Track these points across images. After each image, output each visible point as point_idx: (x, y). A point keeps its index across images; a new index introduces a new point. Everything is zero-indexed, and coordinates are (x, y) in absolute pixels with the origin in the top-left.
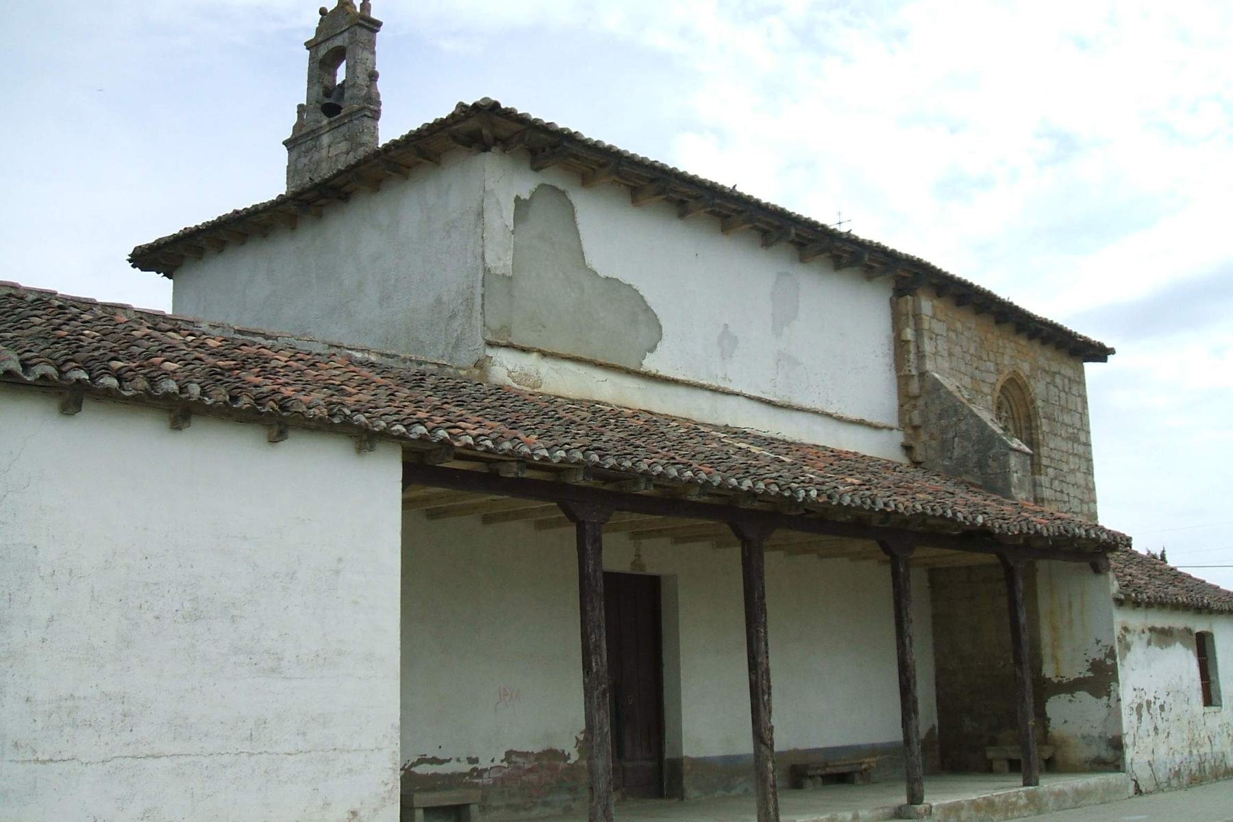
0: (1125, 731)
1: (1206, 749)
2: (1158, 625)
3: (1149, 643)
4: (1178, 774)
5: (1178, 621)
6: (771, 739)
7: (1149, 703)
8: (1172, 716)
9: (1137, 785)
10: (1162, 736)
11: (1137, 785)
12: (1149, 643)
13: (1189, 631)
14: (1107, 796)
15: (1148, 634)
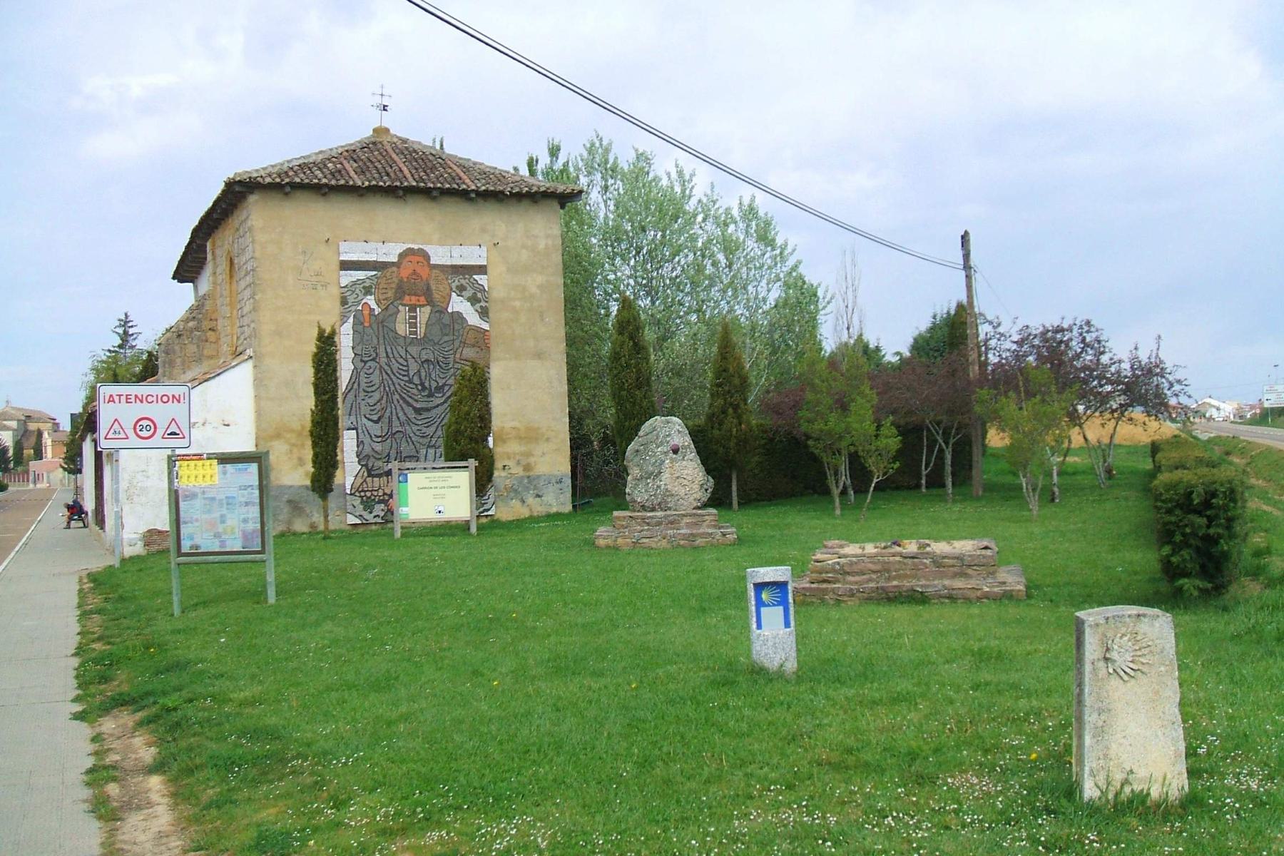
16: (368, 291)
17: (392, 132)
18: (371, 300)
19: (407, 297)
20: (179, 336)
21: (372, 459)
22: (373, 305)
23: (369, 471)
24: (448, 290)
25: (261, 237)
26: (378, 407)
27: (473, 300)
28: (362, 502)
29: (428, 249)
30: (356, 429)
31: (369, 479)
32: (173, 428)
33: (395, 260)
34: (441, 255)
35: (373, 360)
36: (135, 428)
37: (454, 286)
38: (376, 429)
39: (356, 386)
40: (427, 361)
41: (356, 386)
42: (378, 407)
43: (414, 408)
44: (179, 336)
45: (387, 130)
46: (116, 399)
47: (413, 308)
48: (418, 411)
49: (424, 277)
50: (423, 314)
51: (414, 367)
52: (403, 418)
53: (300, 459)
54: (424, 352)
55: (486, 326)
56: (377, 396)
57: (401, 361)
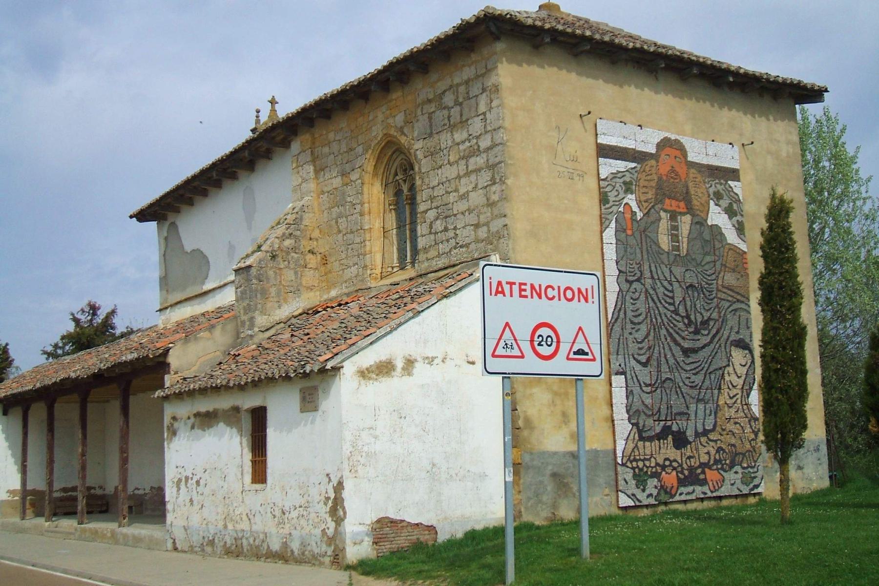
0: (167, 500)
1: (244, 525)
2: (203, 409)
3: (193, 427)
4: (212, 543)
5: (224, 403)
6: (574, 16)
7: (187, 478)
8: (207, 491)
9: (174, 543)
10: (196, 507)
11: (174, 543)
12: (193, 427)
13: (236, 409)
14: (152, 545)
15: (192, 420)
16: (628, 188)
17: (562, 9)
18: (631, 200)
19: (667, 201)
20: (274, 257)
21: (643, 417)
22: (635, 208)
23: (640, 432)
24: (705, 198)
25: (510, 100)
26: (645, 345)
27: (731, 212)
28: (635, 476)
29: (686, 141)
30: (623, 373)
31: (640, 444)
32: (580, 345)
33: (654, 151)
34: (700, 151)
35: (638, 280)
36: (532, 341)
37: (711, 190)
38: (645, 375)
39: (622, 315)
40: (691, 286)
41: (622, 315)
42: (645, 345)
43: (682, 348)
44: (274, 257)
45: (557, 7)
46: (507, 288)
47: (673, 217)
48: (686, 352)
49: (683, 176)
50: (685, 223)
51: (679, 294)
52: (672, 361)
53: (564, 414)
54: (688, 275)
55: (743, 247)
56: (644, 328)
57: (666, 283)
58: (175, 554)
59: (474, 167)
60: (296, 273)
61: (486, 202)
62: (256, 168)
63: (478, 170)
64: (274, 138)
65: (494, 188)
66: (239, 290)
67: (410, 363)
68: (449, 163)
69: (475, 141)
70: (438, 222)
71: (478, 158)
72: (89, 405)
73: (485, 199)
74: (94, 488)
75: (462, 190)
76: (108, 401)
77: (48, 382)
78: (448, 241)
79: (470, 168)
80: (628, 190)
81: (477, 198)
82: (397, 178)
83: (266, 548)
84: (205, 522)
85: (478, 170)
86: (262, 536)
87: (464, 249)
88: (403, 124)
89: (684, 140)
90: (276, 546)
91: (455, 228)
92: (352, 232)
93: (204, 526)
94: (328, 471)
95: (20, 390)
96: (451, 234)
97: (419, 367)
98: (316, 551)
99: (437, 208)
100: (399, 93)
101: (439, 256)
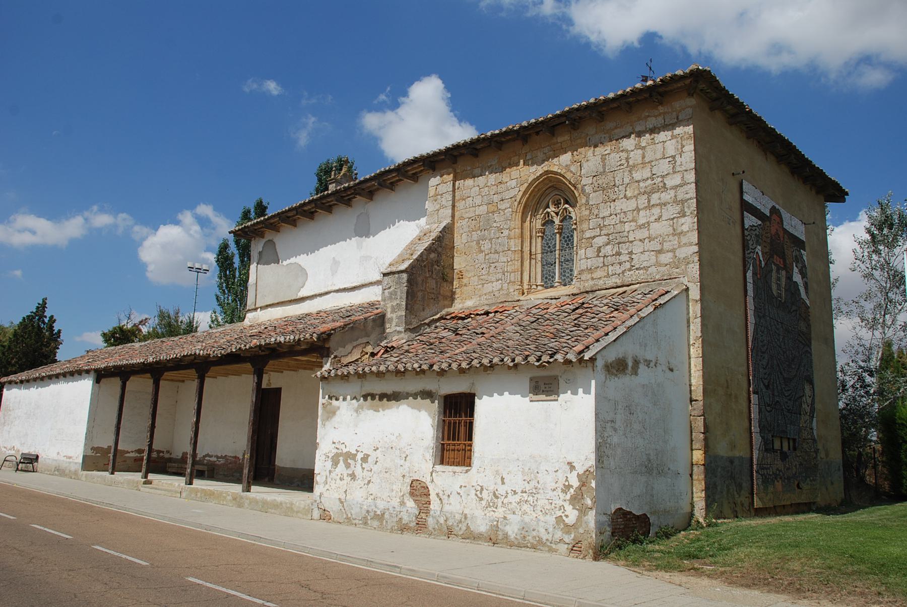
58: (323, 524)
59: (658, 201)
60: (437, 283)
61: (672, 231)
62: (375, 197)
63: (663, 205)
64: (407, 171)
65: (683, 220)
66: (386, 291)
67: (636, 363)
68: (625, 196)
69: (660, 179)
70: (609, 247)
71: (664, 194)
72: (162, 383)
73: (671, 228)
74: (163, 452)
75: (642, 221)
76: (183, 381)
77: (163, 357)
78: (620, 264)
79: (652, 203)
80: (758, 243)
81: (658, 228)
82: (548, 210)
83: (464, 528)
84: (372, 497)
85: (663, 205)
86: (458, 517)
87: (641, 272)
88: (569, 163)
89: (782, 210)
90: (481, 526)
91: (631, 253)
92: (496, 252)
93: (370, 500)
94: (570, 459)
95: (125, 362)
96: (624, 258)
97: (642, 368)
98: (545, 536)
99: (608, 235)
100: (567, 137)
101: (608, 276)
